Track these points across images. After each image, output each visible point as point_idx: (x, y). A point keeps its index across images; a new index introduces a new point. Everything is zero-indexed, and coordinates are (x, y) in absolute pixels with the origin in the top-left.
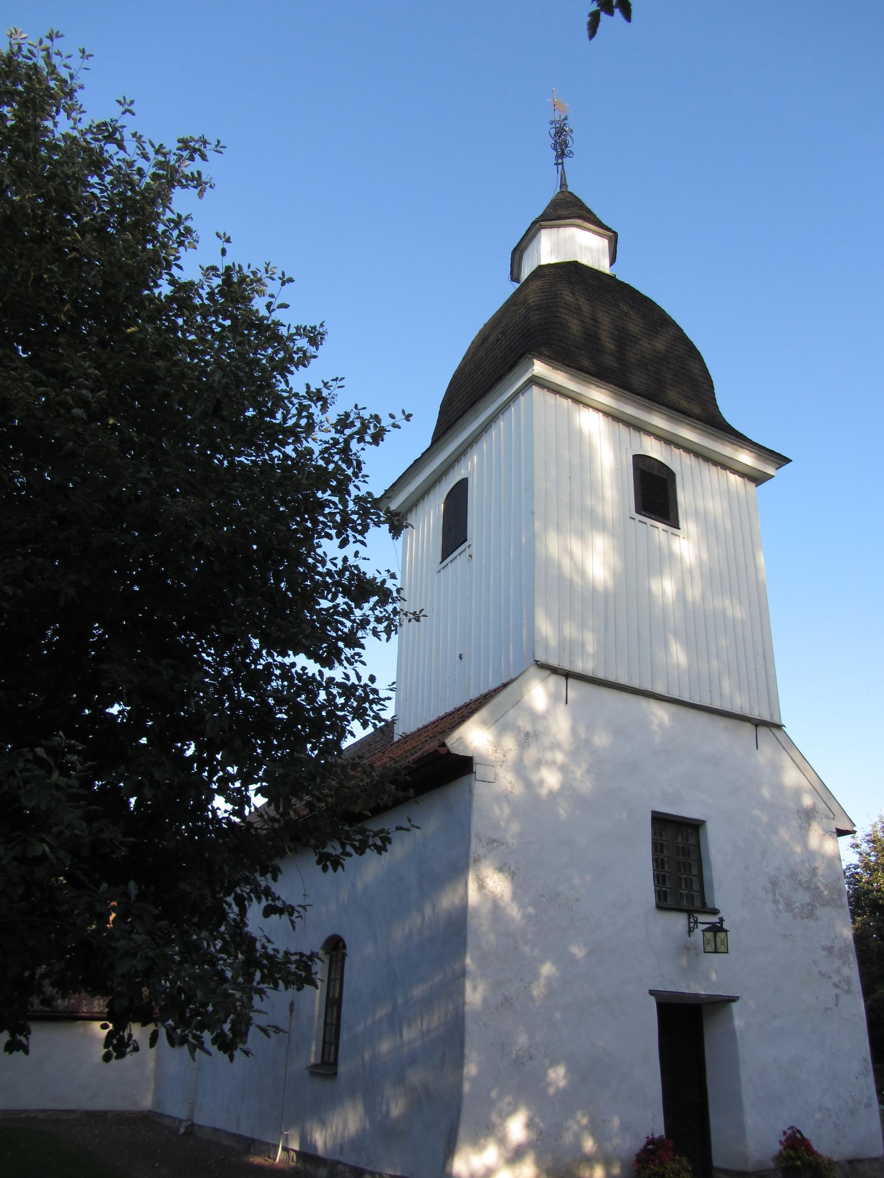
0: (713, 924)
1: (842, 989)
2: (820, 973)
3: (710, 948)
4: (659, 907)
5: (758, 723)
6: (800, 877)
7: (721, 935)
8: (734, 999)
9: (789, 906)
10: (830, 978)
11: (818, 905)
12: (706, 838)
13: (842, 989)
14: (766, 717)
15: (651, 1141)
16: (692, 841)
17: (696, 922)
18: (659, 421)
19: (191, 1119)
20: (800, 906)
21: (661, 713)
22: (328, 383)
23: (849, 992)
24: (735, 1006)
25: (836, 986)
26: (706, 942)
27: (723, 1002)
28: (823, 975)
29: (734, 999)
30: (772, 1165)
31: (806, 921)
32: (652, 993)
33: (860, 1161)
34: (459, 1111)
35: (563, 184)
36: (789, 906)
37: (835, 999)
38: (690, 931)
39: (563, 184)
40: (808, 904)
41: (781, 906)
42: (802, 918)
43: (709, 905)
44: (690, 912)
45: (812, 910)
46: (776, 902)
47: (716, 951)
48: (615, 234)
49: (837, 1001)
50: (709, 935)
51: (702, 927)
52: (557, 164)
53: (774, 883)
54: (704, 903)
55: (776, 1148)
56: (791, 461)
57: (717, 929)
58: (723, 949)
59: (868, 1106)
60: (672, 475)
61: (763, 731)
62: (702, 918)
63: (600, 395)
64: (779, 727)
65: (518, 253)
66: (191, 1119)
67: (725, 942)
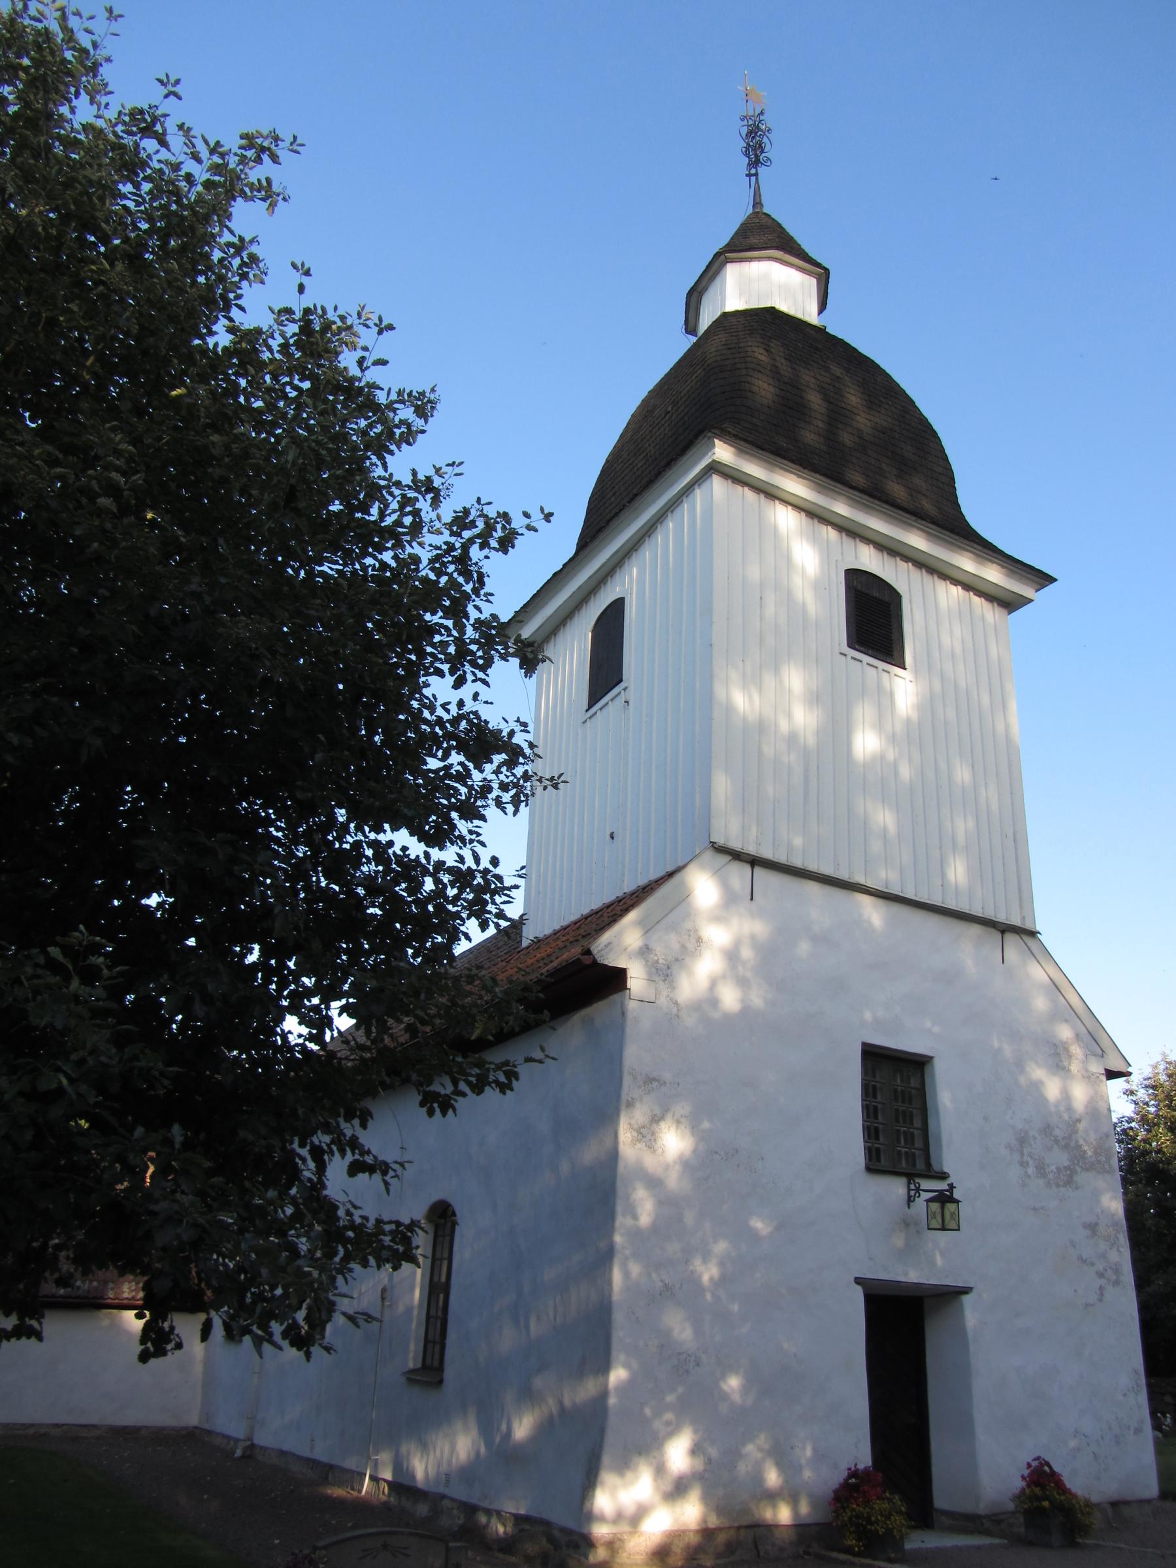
0: (941, 1192)
1: (1108, 1280)
2: (1080, 1258)
3: (936, 1223)
4: (870, 1169)
5: (1005, 929)
6: (1057, 1132)
7: (951, 1207)
8: (966, 1291)
9: (1041, 1169)
10: (1092, 1264)
11: (1079, 1169)
12: (933, 1076)
13: (1108, 1280)
14: (1016, 921)
15: (853, 1474)
16: (914, 1083)
17: (918, 1190)
18: (877, 524)
19: (249, 1439)
20: (1055, 1170)
21: (873, 913)
22: (441, 468)
23: (1117, 1283)
24: (966, 1299)
25: (1100, 1275)
26: (930, 1215)
27: (952, 1295)
28: (1084, 1261)
29: (966, 1291)
30: (1011, 1506)
31: (1062, 1189)
32: (858, 1281)
33: (1127, 1503)
34: (602, 1431)
35: (757, 203)
36: (1041, 1169)
37: (1098, 1292)
38: (910, 1200)
39: (757, 203)
40: (1067, 1168)
41: (1031, 1170)
42: (1058, 1186)
43: (936, 1167)
44: (910, 1176)
45: (1071, 1176)
46: (1023, 1164)
47: (943, 1229)
48: (827, 271)
49: (1102, 1294)
50: (935, 1206)
51: (926, 1196)
52: (749, 175)
53: (1022, 1140)
54: (928, 1164)
55: (1017, 1484)
56: (1055, 580)
57: (945, 1198)
58: (953, 1225)
59: (1138, 1431)
60: (896, 597)
61: (1010, 938)
62: (925, 1184)
63: (794, 485)
64: (1033, 934)
65: (695, 295)
66: (249, 1439)
67: (956, 1216)
